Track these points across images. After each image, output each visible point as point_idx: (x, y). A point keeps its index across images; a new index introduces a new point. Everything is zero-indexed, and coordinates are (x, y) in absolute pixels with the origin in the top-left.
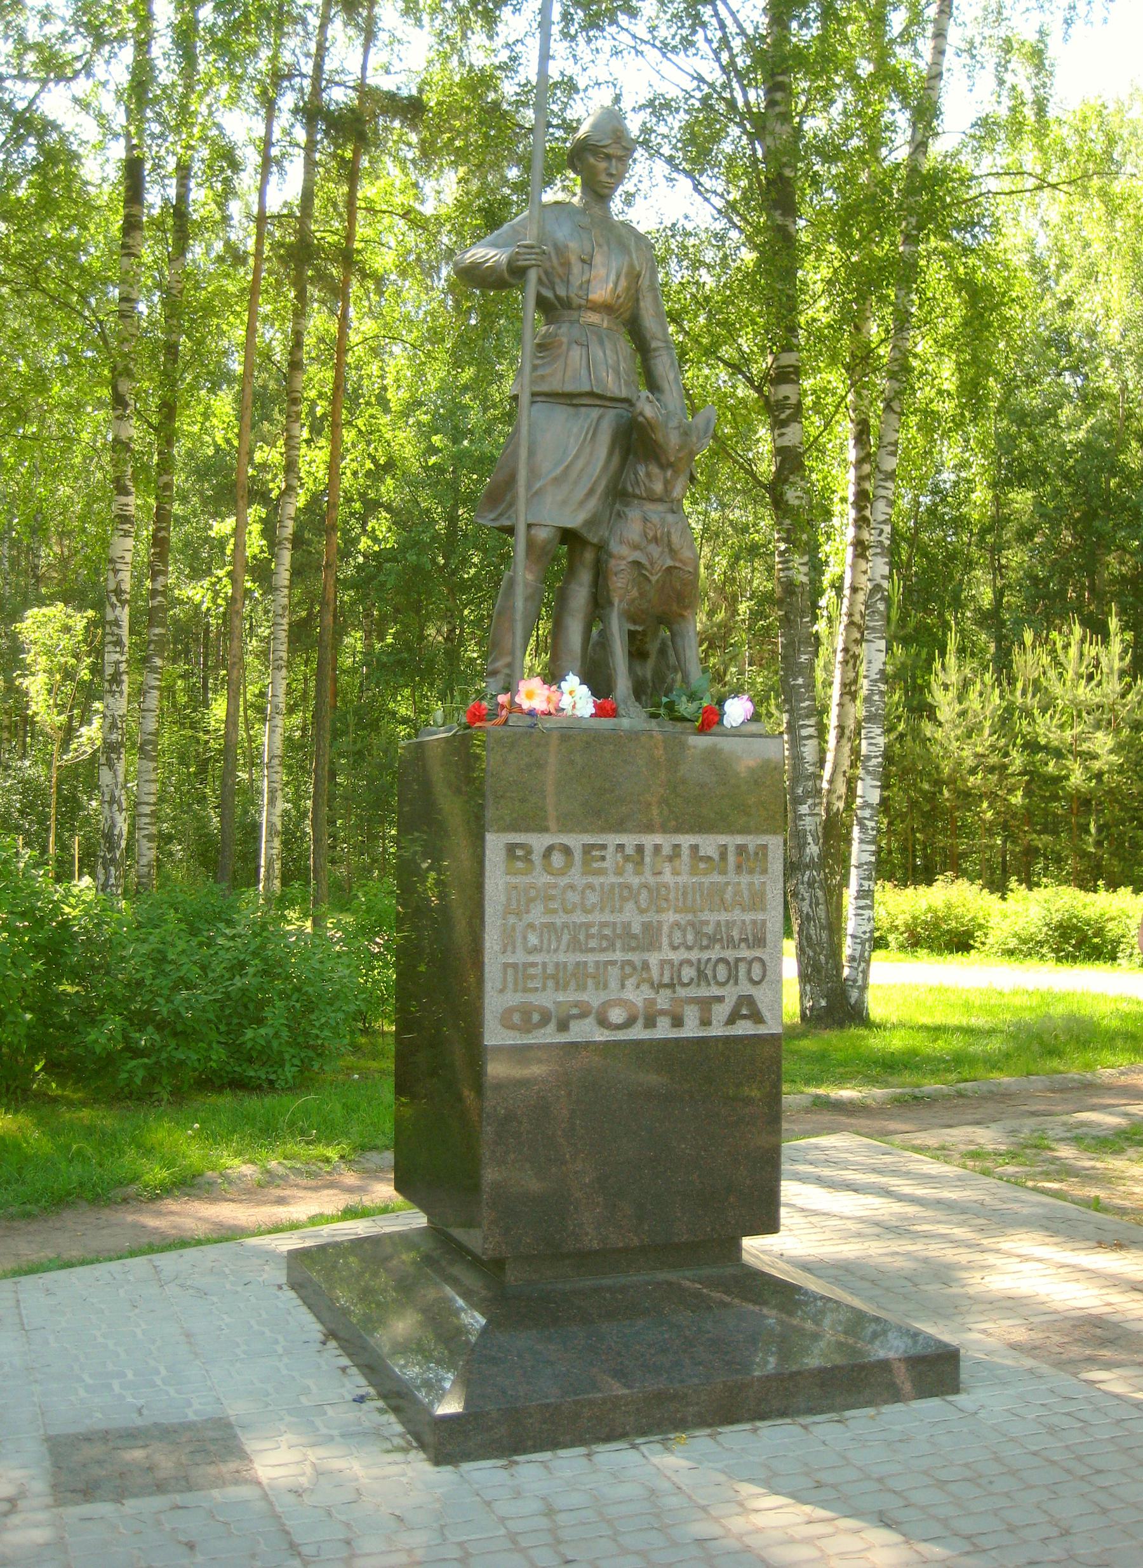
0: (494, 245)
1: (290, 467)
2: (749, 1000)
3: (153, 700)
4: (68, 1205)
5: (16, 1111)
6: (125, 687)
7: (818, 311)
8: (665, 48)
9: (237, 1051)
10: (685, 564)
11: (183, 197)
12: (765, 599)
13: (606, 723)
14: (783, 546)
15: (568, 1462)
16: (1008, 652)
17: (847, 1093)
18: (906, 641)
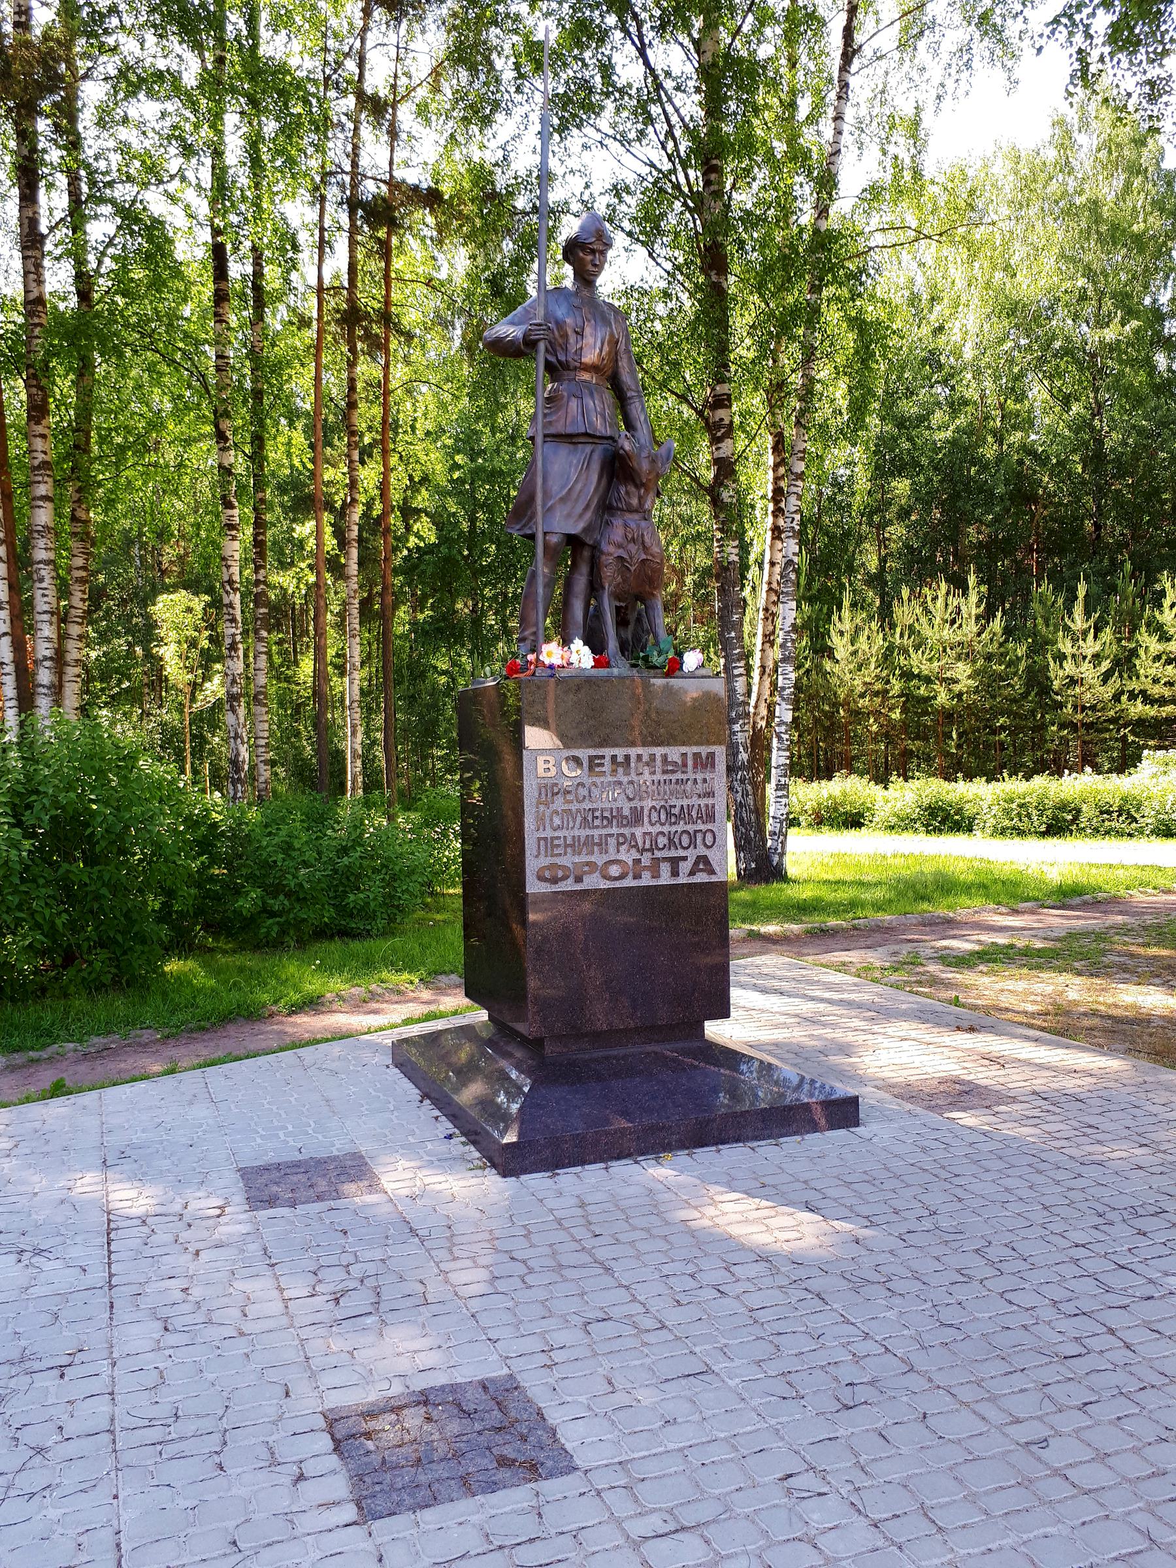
0: (512, 323)
1: (353, 485)
2: (703, 859)
3: (263, 662)
4: (230, 1021)
5: (186, 958)
7: (744, 349)
8: (624, 140)
11: (258, 274)
12: (706, 572)
13: (602, 672)
14: (719, 535)
15: (593, 1173)
16: (890, 605)
17: (771, 928)
18: (811, 600)
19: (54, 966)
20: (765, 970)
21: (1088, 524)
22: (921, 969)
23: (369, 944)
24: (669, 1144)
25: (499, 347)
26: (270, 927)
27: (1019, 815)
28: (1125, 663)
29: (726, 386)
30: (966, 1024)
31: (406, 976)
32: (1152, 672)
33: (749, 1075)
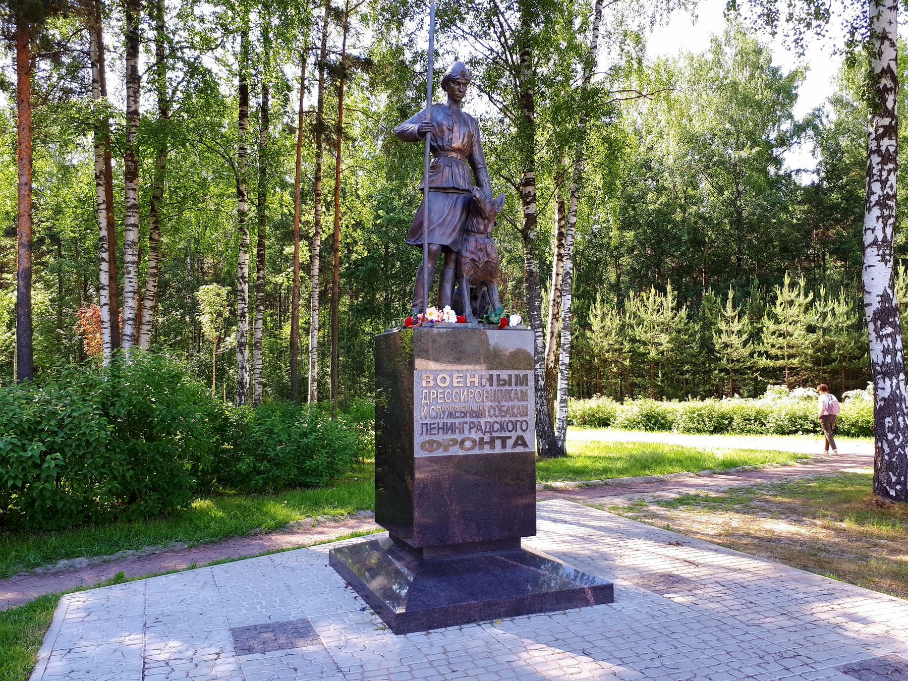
1: (317, 224)
2: (521, 438)
3: (260, 324)
4: (230, 538)
5: (206, 499)
6: (247, 319)
7: (543, 154)
8: (476, 36)
9: (302, 471)
11: (265, 102)
13: (462, 325)
15: (452, 632)
17: (559, 484)
18: (578, 297)
19: (123, 503)
20: (556, 509)
21: (734, 259)
22: (646, 509)
23: (317, 491)
24: (499, 614)
25: (404, 136)
26: (258, 480)
27: (698, 421)
28: (756, 336)
29: (533, 173)
30: (674, 541)
31: (339, 511)
32: (771, 341)
33: (543, 571)
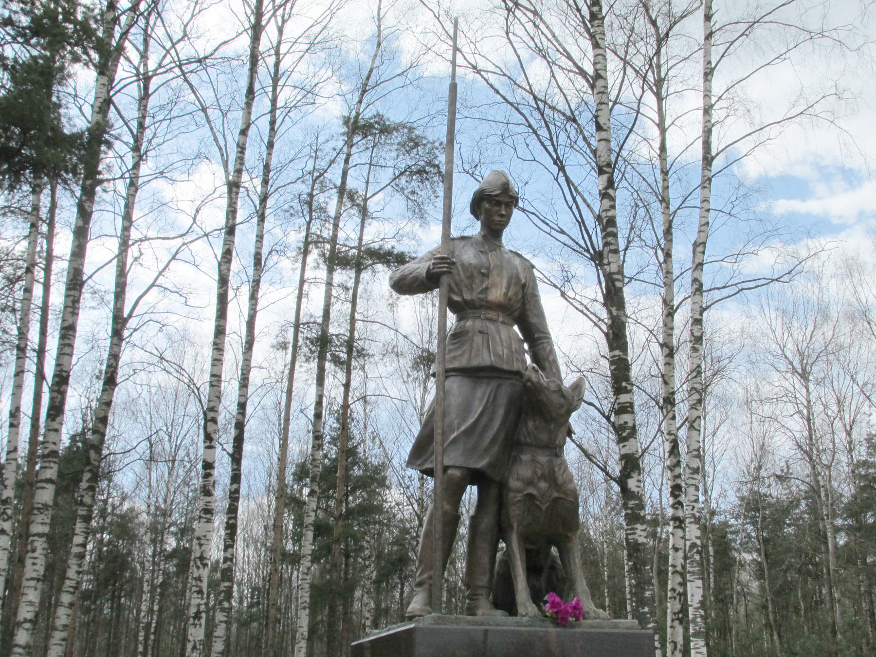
10: (567, 495)
